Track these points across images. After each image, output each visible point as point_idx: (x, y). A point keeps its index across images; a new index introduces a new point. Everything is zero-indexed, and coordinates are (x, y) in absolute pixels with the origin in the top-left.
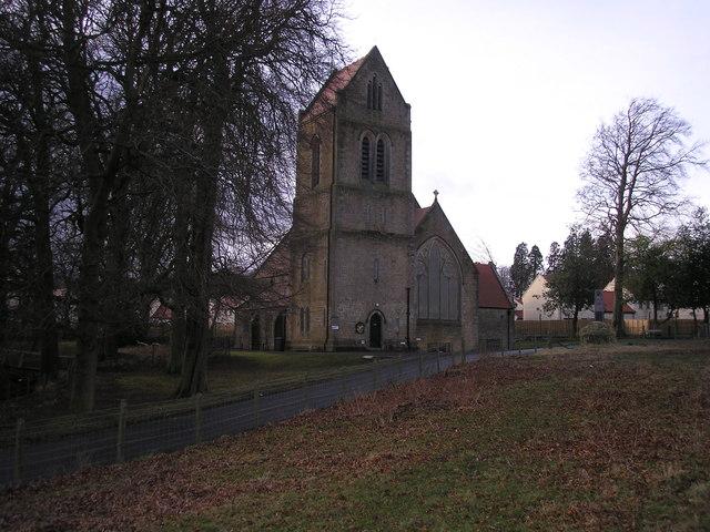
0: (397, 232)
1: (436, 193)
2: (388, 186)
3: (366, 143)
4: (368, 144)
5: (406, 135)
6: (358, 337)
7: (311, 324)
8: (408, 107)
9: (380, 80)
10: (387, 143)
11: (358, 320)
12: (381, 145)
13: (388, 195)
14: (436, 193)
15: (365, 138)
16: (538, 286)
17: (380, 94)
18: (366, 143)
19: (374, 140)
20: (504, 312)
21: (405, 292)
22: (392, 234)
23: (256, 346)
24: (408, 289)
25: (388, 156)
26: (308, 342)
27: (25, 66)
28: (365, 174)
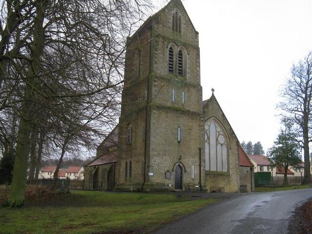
0: (192, 110)
1: (213, 90)
2: (186, 79)
3: (171, 51)
4: (172, 52)
5: (196, 49)
6: (167, 182)
7: (133, 173)
8: (197, 33)
9: (179, 14)
10: (185, 52)
11: (166, 169)
12: (180, 54)
13: (186, 85)
14: (213, 90)
15: (171, 48)
16: (291, 176)
17: (180, 23)
18: (171, 51)
19: (176, 50)
20: (249, 169)
21: (198, 151)
22: (189, 111)
23: (95, 187)
24: (200, 149)
25: (186, 65)
26: (130, 185)
27: (46, 21)
28: (171, 70)
